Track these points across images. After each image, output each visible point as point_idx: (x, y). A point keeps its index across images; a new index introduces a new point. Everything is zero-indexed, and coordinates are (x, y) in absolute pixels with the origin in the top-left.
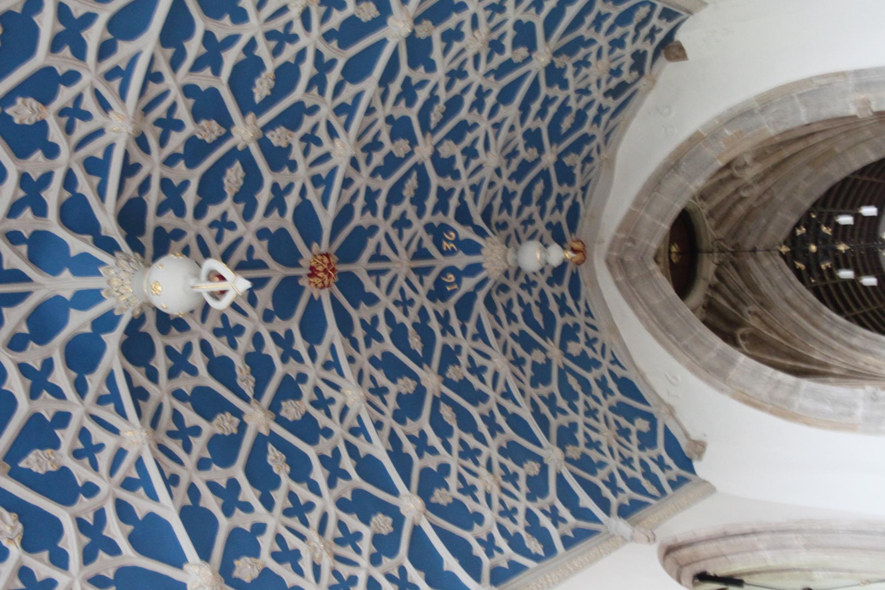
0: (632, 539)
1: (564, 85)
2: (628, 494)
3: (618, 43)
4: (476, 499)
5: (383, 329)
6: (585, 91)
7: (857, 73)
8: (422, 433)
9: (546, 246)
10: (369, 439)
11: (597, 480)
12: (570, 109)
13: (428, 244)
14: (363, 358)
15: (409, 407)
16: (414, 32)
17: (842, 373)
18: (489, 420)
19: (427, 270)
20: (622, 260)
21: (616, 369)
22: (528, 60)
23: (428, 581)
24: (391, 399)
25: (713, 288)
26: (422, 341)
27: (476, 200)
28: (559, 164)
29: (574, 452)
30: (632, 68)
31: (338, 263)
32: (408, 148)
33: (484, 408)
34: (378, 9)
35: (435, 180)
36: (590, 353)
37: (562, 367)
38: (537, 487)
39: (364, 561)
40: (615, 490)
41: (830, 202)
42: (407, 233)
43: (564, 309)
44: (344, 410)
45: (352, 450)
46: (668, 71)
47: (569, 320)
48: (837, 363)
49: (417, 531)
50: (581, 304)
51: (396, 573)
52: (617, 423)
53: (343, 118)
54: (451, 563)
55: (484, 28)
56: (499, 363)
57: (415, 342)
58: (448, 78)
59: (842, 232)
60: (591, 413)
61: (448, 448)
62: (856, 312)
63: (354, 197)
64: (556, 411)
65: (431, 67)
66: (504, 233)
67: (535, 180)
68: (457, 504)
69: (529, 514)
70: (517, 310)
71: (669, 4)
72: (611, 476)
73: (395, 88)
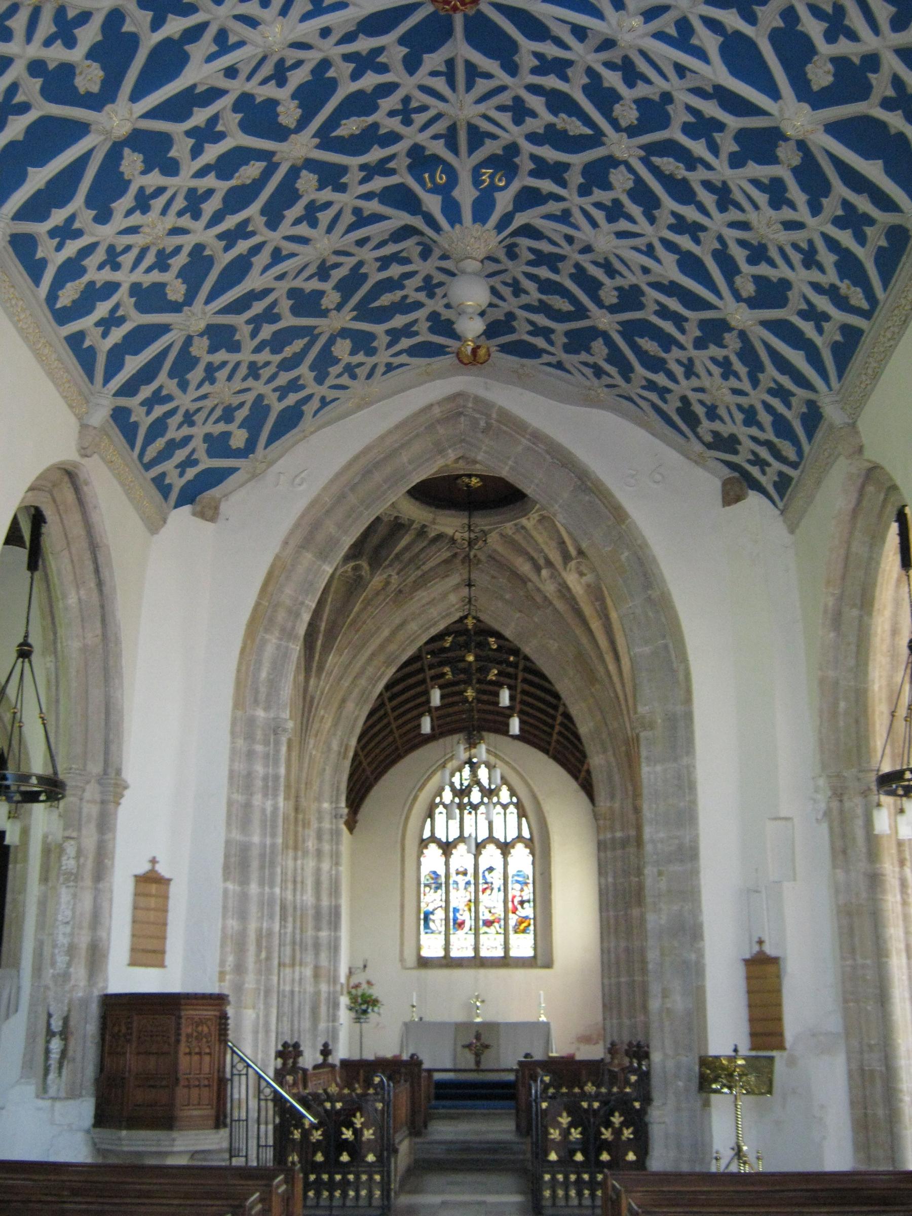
0: (84, 427)
1: (700, 344)
2: (144, 420)
3: (750, 417)
4: (129, 213)
5: (370, 80)
6: (690, 370)
7: (689, 716)
8: (221, 136)
9: (482, 314)
10: (210, 58)
11: (162, 378)
12: (667, 350)
13: (490, 148)
14: (331, 49)
15: (259, 117)
16: (786, 139)
17: (310, 689)
18: (242, 231)
19: (453, 146)
20: (461, 414)
21: (315, 403)
22: (738, 297)
23: (12, 144)
24: (271, 91)
25: (422, 532)
26: (352, 136)
27: (549, 217)
28: (595, 333)
29: (200, 348)
30: (716, 434)
31: (465, 16)
32: (624, 124)
33: (259, 222)
34: (824, 89)
35: (578, 160)
36: (334, 370)
37: (316, 332)
38: (150, 298)
39: (35, 50)
40: (149, 404)
41: (530, 677)
42: (505, 119)
43: (395, 335)
44: (251, 22)
45: (194, 34)
46: (709, 481)
47: (383, 340)
48: (321, 685)
49: (83, 129)
50: (404, 358)
51: (19, 98)
52: (242, 405)
53: (672, 31)
54: (38, 178)
55: (785, 237)
56: (323, 244)
57: (351, 126)
58: (719, 184)
59: (490, 693)
60: (254, 371)
61: (201, 173)
62: (389, 706)
63: (560, 43)
64: (257, 323)
65: (736, 161)
66: (501, 255)
67: (573, 299)
68: (122, 186)
69: (111, 288)
70: (395, 271)
71: (796, 485)
72: (169, 398)
73: (711, 109)
